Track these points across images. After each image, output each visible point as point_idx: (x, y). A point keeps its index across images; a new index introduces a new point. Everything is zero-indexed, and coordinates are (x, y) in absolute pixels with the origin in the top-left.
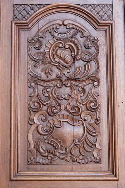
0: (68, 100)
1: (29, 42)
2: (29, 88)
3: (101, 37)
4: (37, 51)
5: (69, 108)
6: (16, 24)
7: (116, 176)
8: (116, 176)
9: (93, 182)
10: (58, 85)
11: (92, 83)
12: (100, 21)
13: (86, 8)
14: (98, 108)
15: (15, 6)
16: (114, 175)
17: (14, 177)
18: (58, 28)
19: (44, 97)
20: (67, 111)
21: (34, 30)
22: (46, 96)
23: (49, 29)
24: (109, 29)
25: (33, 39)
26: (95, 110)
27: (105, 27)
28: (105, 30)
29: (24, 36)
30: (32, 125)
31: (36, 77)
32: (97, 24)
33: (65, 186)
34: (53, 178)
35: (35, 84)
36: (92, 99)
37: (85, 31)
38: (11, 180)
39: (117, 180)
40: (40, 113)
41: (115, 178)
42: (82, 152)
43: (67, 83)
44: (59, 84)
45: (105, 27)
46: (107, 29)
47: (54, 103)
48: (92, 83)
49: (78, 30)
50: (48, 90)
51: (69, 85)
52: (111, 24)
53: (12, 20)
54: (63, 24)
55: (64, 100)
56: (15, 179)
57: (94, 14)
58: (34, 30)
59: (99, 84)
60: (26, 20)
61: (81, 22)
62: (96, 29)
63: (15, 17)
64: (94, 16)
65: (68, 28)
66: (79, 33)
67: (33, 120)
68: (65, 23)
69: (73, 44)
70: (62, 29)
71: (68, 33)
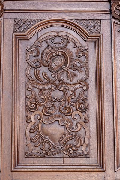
0: (61, 102)
1: (27, 51)
2: (27, 90)
3: (91, 48)
4: (35, 58)
5: (62, 109)
6: (16, 35)
7: (103, 168)
8: (103, 168)
9: (44, 173)
10: (53, 88)
11: (82, 88)
12: (89, 34)
13: (77, 23)
14: (86, 108)
15: (16, 20)
16: (101, 167)
17: (14, 168)
18: (53, 38)
19: (40, 98)
20: (60, 111)
21: (33, 40)
22: (42, 98)
23: (45, 39)
24: (98, 40)
25: (31, 48)
26: (84, 110)
27: (94, 40)
28: (95, 42)
29: (23, 46)
30: (29, 123)
31: (33, 81)
32: (88, 39)
33: (44, 178)
34: (29, 170)
35: (32, 87)
36: (81, 101)
37: (77, 42)
38: (12, 171)
39: (103, 171)
40: (36, 112)
41: (103, 170)
42: (70, 147)
43: (60, 86)
44: (53, 87)
45: (94, 40)
46: (95, 41)
47: (49, 105)
48: (82, 88)
49: (67, 40)
50: (44, 93)
51: (62, 89)
52: (100, 37)
53: (13, 32)
54: (58, 36)
55: (58, 102)
56: (15, 170)
57: (84, 28)
58: (33, 40)
59: (88, 88)
60: (24, 31)
61: (73, 35)
62: (86, 41)
63: (16, 31)
64: (81, 26)
65: (62, 38)
66: (71, 42)
67: (31, 118)
68: (60, 34)
69: (61, 49)
70: (57, 40)
71: (62, 44)
